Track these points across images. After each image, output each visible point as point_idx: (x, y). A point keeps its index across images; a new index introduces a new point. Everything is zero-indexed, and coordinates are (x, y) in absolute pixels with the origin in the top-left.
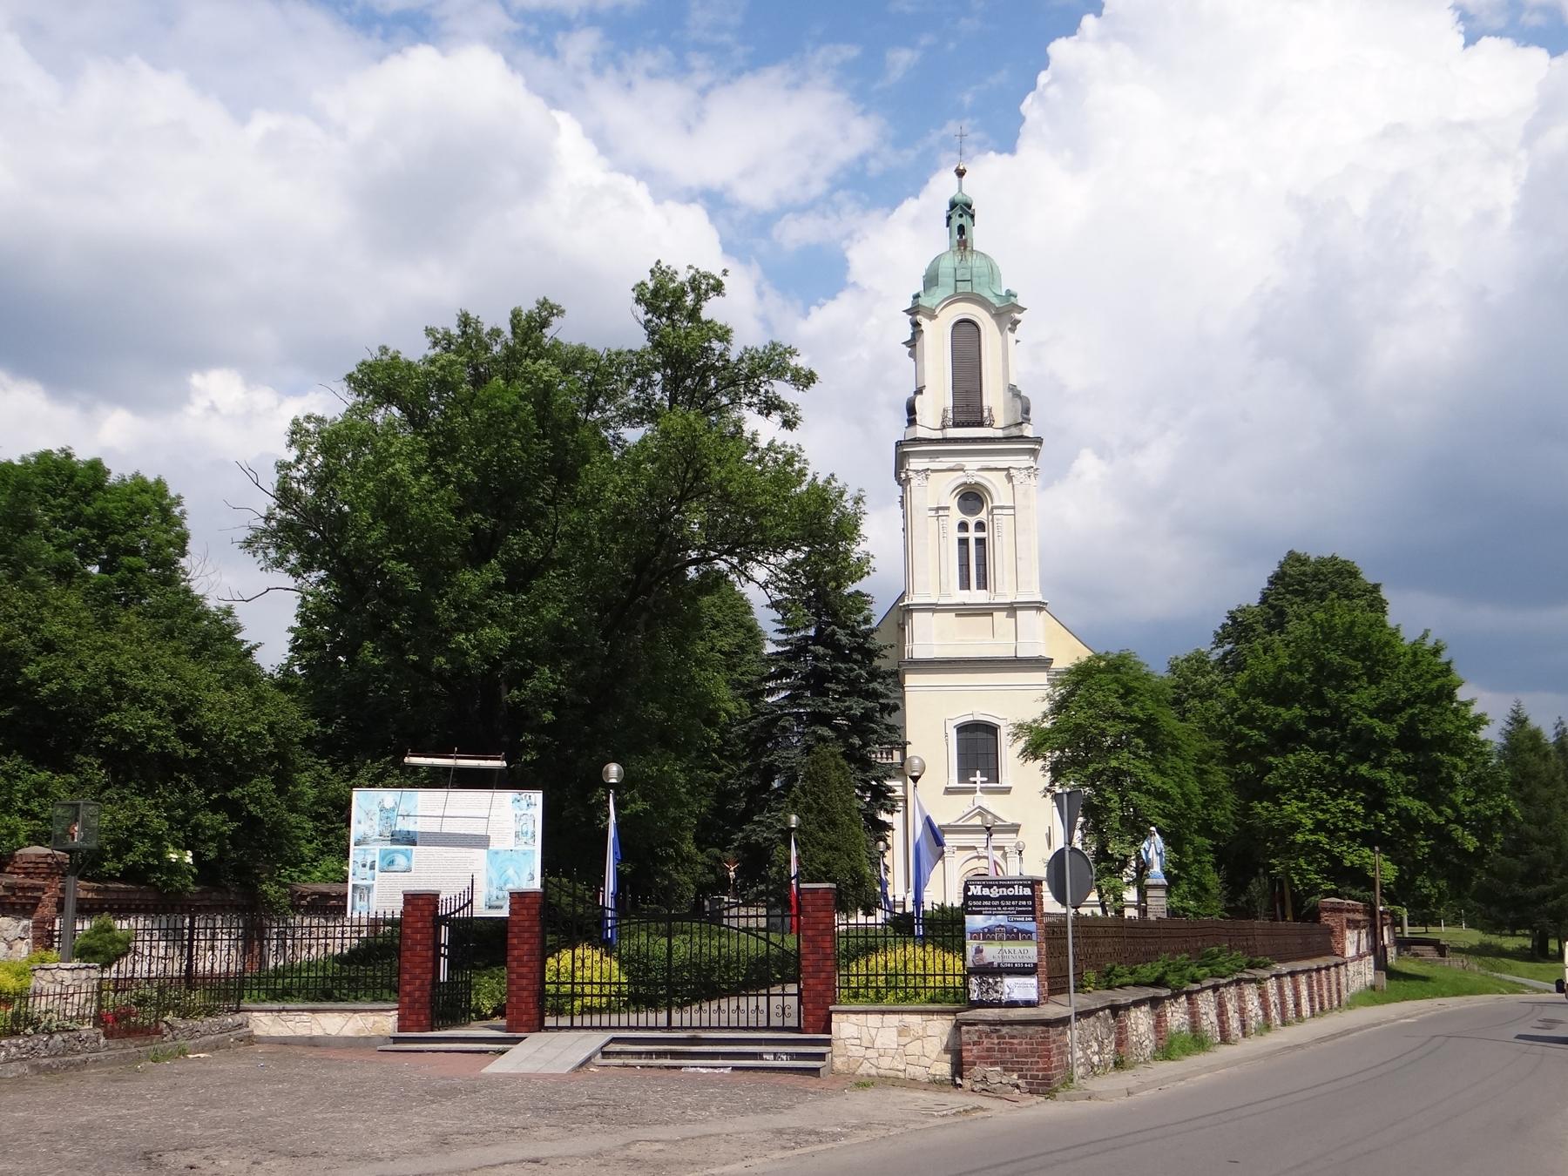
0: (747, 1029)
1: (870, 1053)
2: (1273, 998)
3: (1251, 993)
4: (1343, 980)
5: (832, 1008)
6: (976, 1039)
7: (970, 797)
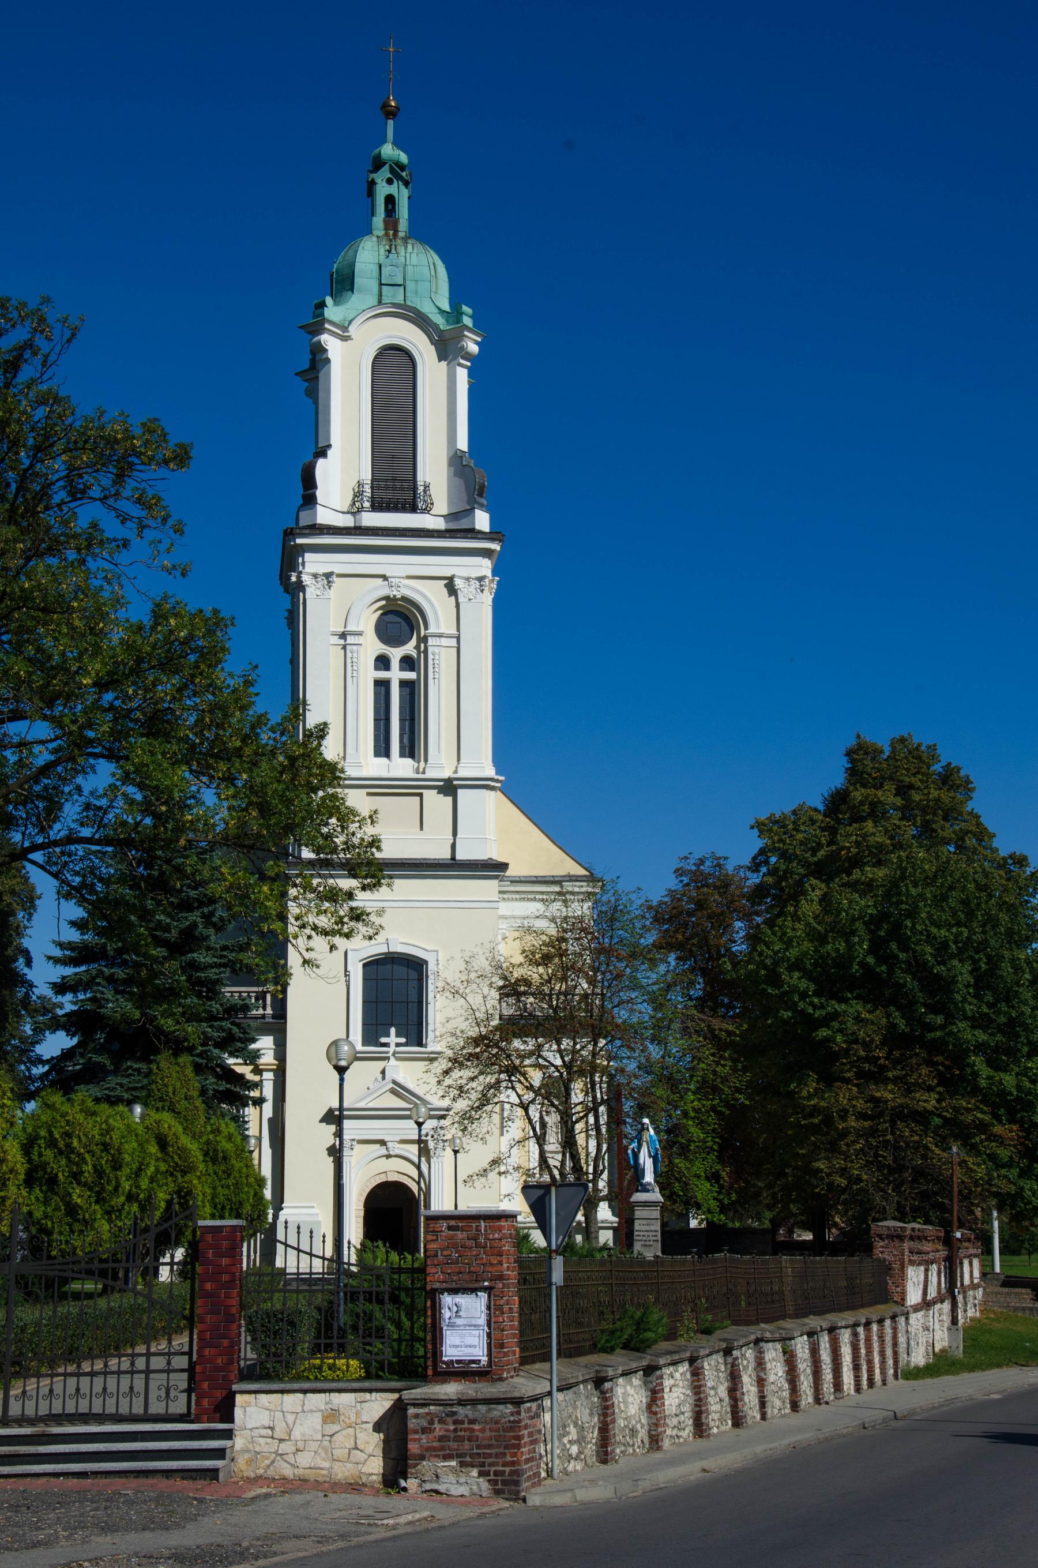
0: (118, 1419)
1: (285, 1447)
2: (804, 1366)
3: (773, 1353)
4: (902, 1339)
5: (235, 1387)
6: (425, 1424)
7: (381, 1065)
